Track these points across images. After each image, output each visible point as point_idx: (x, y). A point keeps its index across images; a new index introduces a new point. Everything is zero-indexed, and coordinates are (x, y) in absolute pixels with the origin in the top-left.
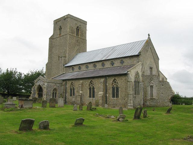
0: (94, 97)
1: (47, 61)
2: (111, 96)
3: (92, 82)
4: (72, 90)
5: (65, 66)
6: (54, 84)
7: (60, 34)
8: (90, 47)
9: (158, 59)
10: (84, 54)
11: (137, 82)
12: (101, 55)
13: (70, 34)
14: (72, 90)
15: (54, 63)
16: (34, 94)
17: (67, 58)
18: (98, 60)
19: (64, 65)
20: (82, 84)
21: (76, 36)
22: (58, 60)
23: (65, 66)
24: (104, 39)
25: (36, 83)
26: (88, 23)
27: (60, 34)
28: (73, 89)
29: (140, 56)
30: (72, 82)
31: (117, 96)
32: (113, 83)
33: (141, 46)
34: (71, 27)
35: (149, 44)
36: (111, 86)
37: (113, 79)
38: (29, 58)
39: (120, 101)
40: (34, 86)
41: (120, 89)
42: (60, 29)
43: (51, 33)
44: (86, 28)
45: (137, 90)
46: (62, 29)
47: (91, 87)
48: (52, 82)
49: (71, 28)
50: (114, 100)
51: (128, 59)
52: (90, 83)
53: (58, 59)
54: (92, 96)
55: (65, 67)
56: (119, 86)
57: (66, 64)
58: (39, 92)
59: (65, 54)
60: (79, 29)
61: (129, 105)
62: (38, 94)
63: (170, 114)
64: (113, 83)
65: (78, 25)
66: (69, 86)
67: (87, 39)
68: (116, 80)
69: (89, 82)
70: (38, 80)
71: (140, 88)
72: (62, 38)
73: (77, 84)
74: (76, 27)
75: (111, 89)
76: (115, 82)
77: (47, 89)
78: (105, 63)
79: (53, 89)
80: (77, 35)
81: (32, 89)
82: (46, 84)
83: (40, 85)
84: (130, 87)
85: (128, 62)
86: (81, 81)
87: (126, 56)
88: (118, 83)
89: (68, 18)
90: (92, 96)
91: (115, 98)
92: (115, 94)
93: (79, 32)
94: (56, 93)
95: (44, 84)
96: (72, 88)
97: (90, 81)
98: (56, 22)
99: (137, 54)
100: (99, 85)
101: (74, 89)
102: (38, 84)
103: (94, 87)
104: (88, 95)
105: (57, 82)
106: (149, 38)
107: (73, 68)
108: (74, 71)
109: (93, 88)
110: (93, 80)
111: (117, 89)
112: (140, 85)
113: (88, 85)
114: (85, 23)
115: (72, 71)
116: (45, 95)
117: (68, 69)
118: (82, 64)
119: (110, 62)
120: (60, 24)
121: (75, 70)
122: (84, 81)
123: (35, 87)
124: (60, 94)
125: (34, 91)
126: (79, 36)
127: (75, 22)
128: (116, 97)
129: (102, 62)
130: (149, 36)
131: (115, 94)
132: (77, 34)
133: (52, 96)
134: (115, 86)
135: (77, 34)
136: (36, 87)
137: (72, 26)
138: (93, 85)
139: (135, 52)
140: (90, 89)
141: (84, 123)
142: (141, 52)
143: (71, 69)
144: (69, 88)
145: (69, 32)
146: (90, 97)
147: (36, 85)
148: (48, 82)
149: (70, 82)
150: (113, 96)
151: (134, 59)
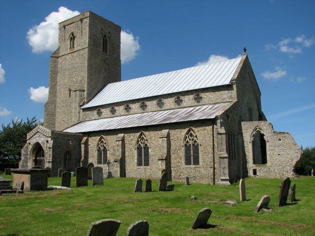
0: (147, 164)
2: (183, 161)
3: (143, 136)
4: (143, 149)
5: (82, 107)
9: (260, 94)
11: (231, 135)
14: (143, 149)
16: (26, 161)
17: (86, 92)
18: (151, 95)
23: (82, 107)
28: (144, 148)
31: (197, 162)
32: (187, 136)
33: (233, 68)
36: (182, 143)
39: (202, 170)
45: (232, 149)
46: (76, 39)
47: (142, 146)
50: (191, 168)
53: (68, 94)
54: (143, 163)
58: (36, 157)
68: (103, 138)
70: (35, 135)
71: (236, 146)
72: (75, 54)
73: (112, 142)
75: (183, 149)
76: (191, 135)
81: (23, 152)
83: (38, 144)
84: (222, 144)
87: (190, 89)
88: (196, 136)
90: (143, 163)
92: (192, 157)
93: (108, 44)
96: (102, 148)
99: (227, 82)
100: (156, 142)
101: (105, 150)
102: (33, 141)
104: (136, 161)
107: (99, 110)
108: (102, 117)
111: (196, 148)
112: (235, 140)
113: (134, 142)
115: (96, 116)
123: (27, 147)
125: (26, 155)
131: (192, 157)
132: (105, 49)
133: (62, 163)
136: (30, 147)
138: (105, 145)
139: (218, 80)
141: (210, 221)
144: (95, 149)
146: (139, 164)
147: (30, 143)
150: (188, 162)
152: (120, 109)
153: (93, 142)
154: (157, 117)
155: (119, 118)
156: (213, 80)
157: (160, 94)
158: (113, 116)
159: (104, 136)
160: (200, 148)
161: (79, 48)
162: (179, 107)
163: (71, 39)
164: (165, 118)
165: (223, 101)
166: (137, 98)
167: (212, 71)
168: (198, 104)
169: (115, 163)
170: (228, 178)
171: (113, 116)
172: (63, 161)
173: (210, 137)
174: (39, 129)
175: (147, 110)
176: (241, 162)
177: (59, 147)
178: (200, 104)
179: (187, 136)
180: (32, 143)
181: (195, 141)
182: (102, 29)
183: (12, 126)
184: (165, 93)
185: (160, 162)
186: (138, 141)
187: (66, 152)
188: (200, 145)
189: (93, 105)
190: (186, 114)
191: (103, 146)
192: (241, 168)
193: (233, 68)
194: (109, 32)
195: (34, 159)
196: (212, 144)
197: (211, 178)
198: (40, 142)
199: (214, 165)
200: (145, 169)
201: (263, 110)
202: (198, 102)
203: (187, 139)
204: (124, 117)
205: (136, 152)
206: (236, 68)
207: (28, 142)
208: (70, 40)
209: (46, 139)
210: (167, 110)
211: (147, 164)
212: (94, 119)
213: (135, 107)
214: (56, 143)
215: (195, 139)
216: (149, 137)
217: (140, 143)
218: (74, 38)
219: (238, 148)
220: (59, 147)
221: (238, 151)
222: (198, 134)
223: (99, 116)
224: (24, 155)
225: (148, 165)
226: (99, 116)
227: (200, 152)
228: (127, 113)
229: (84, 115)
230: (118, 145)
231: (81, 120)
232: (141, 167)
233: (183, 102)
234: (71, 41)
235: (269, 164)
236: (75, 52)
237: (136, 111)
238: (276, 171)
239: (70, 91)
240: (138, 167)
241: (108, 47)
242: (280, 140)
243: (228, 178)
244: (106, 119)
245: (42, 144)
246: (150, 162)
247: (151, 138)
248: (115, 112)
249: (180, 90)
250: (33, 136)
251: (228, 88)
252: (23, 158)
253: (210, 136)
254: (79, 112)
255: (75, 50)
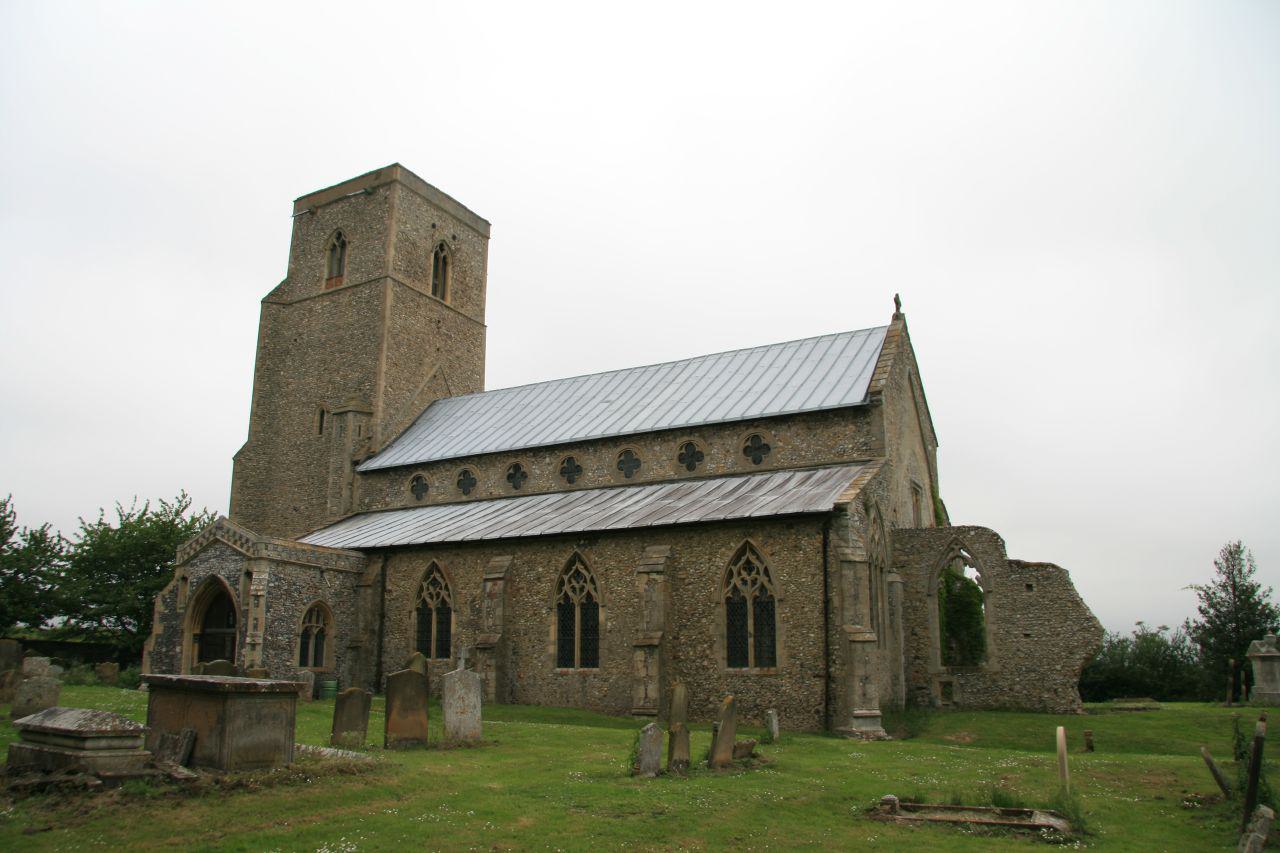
1: (240, 436)
2: (720, 653)
5: (362, 468)
6: (312, 572)
7: (336, 275)
8: (508, 357)
10: (473, 403)
12: (612, 398)
13: (400, 277)
15: (285, 449)
16: (172, 636)
19: (356, 463)
20: (508, 578)
21: (430, 294)
22: (316, 430)
24: (605, 309)
25: (185, 564)
26: (494, 232)
27: (336, 275)
28: (438, 611)
29: (875, 412)
30: (434, 567)
31: (767, 658)
32: (735, 569)
34: (404, 239)
35: (897, 344)
37: (735, 545)
38: (132, 411)
39: (786, 686)
40: (170, 586)
41: (781, 613)
42: (340, 244)
43: (276, 271)
44: (483, 255)
46: (349, 249)
47: (576, 599)
48: (303, 561)
49: (408, 245)
50: (745, 678)
51: (794, 429)
52: (567, 570)
55: (365, 473)
56: (776, 590)
57: (371, 456)
58: (204, 626)
59: (367, 398)
60: (449, 260)
61: (858, 712)
62: (201, 639)
63: (832, 742)
64: (731, 574)
65: (446, 232)
66: (413, 593)
67: (258, 329)
69: (561, 567)
72: (344, 299)
74: (428, 245)
76: (749, 567)
77: (268, 608)
78: (641, 452)
79: (305, 609)
80: (434, 293)
82: (262, 575)
83: (214, 580)
84: (856, 597)
85: (795, 449)
86: (503, 561)
88: (766, 571)
89: (383, 186)
91: (752, 670)
92: (751, 641)
94: (321, 635)
95: (249, 574)
97: (563, 560)
98: (309, 209)
99: (856, 397)
101: (445, 612)
102: (201, 571)
103: (598, 598)
104: (553, 649)
105: (332, 564)
106: (898, 317)
108: (426, 500)
109: (590, 608)
110: (591, 556)
111: (765, 608)
113: (545, 586)
114: (479, 229)
115: (407, 496)
116: (253, 646)
117: (381, 483)
118: (480, 457)
119: (675, 447)
120: (334, 217)
121: (432, 492)
122: (521, 557)
123: (174, 593)
124: (347, 642)
125: (172, 616)
126: (448, 302)
127: (430, 216)
128: (759, 663)
129: (624, 447)
130: (898, 308)
131: (751, 641)
132: (439, 288)
133: (297, 652)
134: (748, 593)
135: (439, 288)
136: (187, 591)
137: (413, 236)
138: (443, 593)
140: (565, 611)
142: (879, 392)
143: (406, 486)
144: (412, 604)
145: (377, 269)
146: (565, 658)
147: (184, 579)
148: (278, 563)
149: (421, 566)
150: (736, 657)
151: (837, 429)
152: (491, 479)
153: (405, 583)
154: (630, 507)
155: (485, 505)
156: (715, 402)
157: (629, 429)
158: (464, 498)
159: (441, 564)
160: (778, 611)
161: (358, 278)
162: (693, 474)
163: (333, 248)
164: (653, 508)
165: (839, 460)
166: (550, 440)
167: (725, 377)
168: (754, 467)
169: (479, 655)
170: (878, 712)
171: (464, 498)
172: (299, 640)
173: (814, 576)
174: (220, 532)
175: (581, 482)
176: (903, 659)
177: (288, 593)
178: (762, 466)
179: (566, 578)
180: (191, 579)
181: (763, 588)
182: (434, 226)
183: (116, 525)
184: (647, 427)
185: (640, 655)
186: (562, 583)
187: (310, 611)
188: (781, 601)
189: (400, 462)
190: (725, 497)
191: (438, 595)
192: (902, 678)
193: (865, 355)
194: (454, 238)
195: (197, 631)
196: (821, 597)
197: (817, 712)
198: (222, 576)
199: (828, 667)
200: (584, 676)
201: (942, 495)
202: (757, 461)
203: (736, 580)
204: (503, 503)
205: (553, 619)
206: (876, 356)
207: (178, 573)
208: (328, 253)
209: (244, 565)
210: (651, 483)
211: (591, 659)
212: (399, 505)
213: (719, 455)
214: (278, 579)
215: (589, 587)
216: (601, 570)
217: (566, 588)
218: (343, 245)
219: (892, 614)
220: (288, 593)
221: (892, 622)
222: (772, 563)
223: (419, 498)
224: (164, 618)
225: (595, 665)
226: (419, 498)
227: (778, 625)
228: (514, 492)
229: (367, 493)
230: (491, 596)
231: (356, 508)
232: (571, 670)
233: (707, 459)
234: (332, 256)
235: (991, 665)
236: (345, 289)
237: (543, 483)
238: (1017, 687)
239: (322, 414)
240: (559, 670)
241: (450, 282)
242: (1029, 587)
243: (878, 712)
244: (442, 509)
245: (227, 582)
246: (603, 651)
247: (605, 575)
248: (639, 466)
249: (698, 420)
250: (195, 556)
251: (855, 417)
252: (158, 628)
253: (812, 570)
254: (351, 484)
255: (346, 283)
